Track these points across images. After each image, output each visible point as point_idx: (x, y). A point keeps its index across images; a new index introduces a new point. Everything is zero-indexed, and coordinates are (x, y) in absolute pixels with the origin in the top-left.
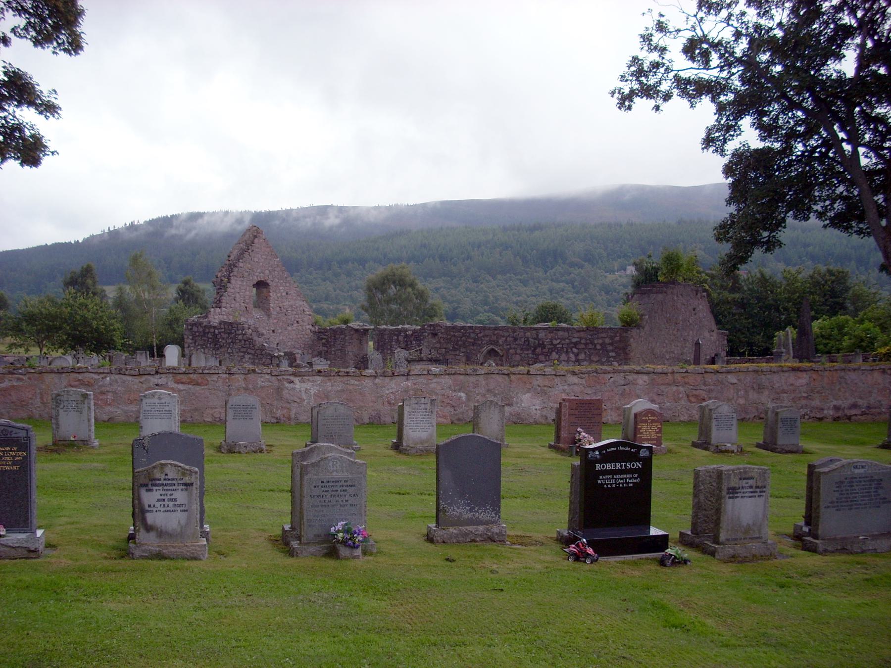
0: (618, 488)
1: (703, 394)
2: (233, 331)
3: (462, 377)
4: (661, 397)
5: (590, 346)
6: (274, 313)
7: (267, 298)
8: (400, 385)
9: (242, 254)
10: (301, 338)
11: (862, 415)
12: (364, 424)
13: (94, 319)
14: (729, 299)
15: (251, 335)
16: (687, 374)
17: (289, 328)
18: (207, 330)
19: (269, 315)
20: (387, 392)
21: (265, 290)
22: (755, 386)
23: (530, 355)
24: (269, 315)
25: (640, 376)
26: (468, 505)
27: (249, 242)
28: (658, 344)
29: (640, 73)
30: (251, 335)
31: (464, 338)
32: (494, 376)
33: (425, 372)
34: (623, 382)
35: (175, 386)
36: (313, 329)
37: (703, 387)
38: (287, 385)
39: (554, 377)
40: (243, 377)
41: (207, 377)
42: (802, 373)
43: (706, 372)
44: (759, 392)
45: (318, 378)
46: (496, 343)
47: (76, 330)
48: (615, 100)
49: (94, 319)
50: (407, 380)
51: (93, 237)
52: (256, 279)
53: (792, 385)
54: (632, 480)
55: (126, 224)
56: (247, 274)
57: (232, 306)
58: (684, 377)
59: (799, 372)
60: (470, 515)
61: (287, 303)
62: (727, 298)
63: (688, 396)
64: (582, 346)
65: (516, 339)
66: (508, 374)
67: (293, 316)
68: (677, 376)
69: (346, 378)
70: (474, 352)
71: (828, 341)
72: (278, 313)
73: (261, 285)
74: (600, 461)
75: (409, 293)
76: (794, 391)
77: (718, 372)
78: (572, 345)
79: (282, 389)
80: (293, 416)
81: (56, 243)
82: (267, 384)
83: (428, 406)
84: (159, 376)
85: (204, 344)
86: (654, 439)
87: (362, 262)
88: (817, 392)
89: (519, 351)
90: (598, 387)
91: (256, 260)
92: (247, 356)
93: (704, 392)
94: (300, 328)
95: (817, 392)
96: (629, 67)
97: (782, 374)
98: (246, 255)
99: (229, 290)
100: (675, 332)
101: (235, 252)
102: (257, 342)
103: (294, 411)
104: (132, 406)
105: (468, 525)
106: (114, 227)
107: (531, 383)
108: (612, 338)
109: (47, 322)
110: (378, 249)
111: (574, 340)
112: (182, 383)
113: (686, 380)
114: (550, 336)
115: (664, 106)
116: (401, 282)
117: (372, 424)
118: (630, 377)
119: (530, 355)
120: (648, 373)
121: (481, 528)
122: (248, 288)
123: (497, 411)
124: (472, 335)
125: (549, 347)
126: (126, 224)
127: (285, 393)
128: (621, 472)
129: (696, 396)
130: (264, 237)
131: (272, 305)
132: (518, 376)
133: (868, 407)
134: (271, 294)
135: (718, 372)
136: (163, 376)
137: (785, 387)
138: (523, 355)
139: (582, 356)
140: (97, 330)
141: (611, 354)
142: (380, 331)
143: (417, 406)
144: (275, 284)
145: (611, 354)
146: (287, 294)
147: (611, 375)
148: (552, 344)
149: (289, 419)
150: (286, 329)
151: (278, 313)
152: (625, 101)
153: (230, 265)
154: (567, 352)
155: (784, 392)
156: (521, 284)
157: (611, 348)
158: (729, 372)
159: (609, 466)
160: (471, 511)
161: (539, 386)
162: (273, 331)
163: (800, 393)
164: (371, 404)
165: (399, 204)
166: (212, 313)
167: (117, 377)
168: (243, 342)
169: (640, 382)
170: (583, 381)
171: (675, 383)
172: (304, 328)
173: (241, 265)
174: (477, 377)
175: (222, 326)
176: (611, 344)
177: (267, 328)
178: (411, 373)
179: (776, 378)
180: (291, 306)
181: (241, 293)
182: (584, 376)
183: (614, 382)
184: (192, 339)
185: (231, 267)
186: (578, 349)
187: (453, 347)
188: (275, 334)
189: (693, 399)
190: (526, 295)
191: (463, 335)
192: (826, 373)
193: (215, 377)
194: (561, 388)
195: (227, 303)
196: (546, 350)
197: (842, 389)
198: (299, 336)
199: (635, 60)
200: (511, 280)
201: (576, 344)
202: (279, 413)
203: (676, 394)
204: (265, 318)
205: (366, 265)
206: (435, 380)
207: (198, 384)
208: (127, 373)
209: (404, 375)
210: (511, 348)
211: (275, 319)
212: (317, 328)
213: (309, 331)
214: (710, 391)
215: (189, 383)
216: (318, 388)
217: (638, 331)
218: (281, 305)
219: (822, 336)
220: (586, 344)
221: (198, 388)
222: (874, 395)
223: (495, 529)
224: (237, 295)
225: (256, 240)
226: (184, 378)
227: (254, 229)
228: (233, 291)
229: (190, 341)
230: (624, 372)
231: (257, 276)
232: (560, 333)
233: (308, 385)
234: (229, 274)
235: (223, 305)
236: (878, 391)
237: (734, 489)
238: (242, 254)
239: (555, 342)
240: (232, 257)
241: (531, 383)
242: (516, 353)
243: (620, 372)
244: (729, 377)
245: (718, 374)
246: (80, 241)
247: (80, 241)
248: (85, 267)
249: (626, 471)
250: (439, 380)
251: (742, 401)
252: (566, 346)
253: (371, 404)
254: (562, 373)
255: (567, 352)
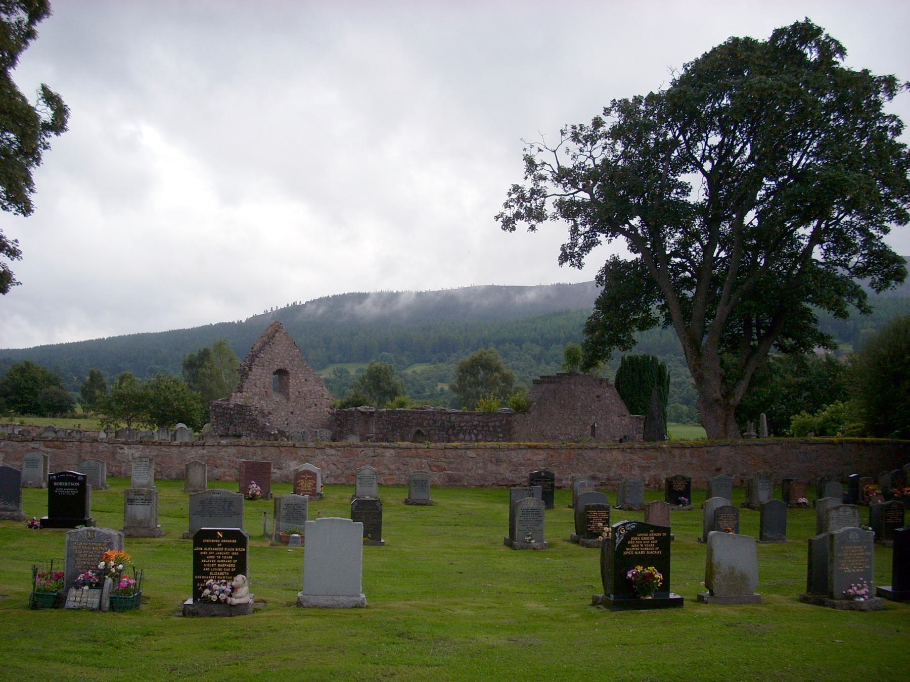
0: (66, 495)
1: (444, 465)
2: (243, 412)
3: (243, 448)
4: (406, 467)
5: (486, 428)
6: (292, 397)
7: (287, 385)
8: (198, 452)
9: (264, 346)
10: (319, 419)
11: (601, 485)
12: (172, 479)
13: (176, 400)
14: (792, 382)
15: (257, 416)
16: (428, 450)
17: (307, 410)
18: (226, 412)
19: (288, 399)
20: (189, 457)
21: (285, 377)
22: (493, 459)
23: (445, 436)
24: (288, 399)
25: (388, 450)
26: (3, 501)
27: (271, 336)
28: (549, 427)
29: (522, 198)
30: (257, 416)
31: (399, 421)
32: (267, 447)
33: (216, 444)
34: (372, 455)
35: (44, 449)
36: (331, 411)
37: (444, 460)
38: (119, 450)
39: (315, 449)
40: (89, 444)
41: (66, 444)
42: (539, 450)
43: (445, 448)
44: (497, 465)
45: (139, 446)
46: (421, 425)
47: (159, 409)
48: (500, 223)
49: (176, 400)
50: (203, 449)
51: (255, 318)
52: (276, 368)
53: (529, 460)
54: (74, 492)
55: (288, 305)
56: (267, 363)
57: (253, 390)
58: (426, 452)
59: (536, 450)
60: (4, 506)
61: (306, 388)
62: (791, 381)
63: (430, 466)
64: (480, 428)
65: (435, 422)
66: (278, 447)
67: (311, 400)
68: (420, 450)
69: (159, 447)
70: (406, 432)
71: (837, 425)
72: (297, 397)
73: (281, 373)
74: (57, 481)
75: (496, 377)
76: (532, 465)
77: (457, 448)
78: (473, 427)
79: (116, 453)
80: (123, 472)
81: (220, 324)
82: (105, 449)
83: (148, 463)
84: (34, 442)
85: (223, 423)
86: (310, 491)
87: (519, 342)
88: (555, 466)
89: (437, 432)
90: (352, 457)
91: (276, 351)
92: (252, 434)
93: (445, 464)
94: (318, 410)
95: (555, 466)
96: (510, 194)
97: (519, 451)
98: (267, 347)
99: (250, 377)
100: (571, 417)
101: (258, 345)
102: (260, 422)
103: (123, 469)
104: (17, 462)
105: (3, 511)
106: (277, 308)
107: (296, 454)
108: (501, 421)
109: (133, 402)
110: (535, 330)
111: (475, 423)
112: (49, 447)
113: (428, 454)
114: (458, 419)
115: (539, 226)
116: (486, 365)
117: (178, 479)
118: (379, 451)
119: (445, 436)
120: (394, 448)
121: (9, 513)
122: (268, 376)
123: (200, 468)
124: (405, 418)
125: (458, 428)
126: (288, 305)
127: (118, 456)
128: (67, 487)
129: (438, 466)
130: (284, 332)
131: (291, 390)
132: (287, 448)
133: (608, 479)
134: (290, 381)
135: (457, 448)
136: (37, 442)
137: (523, 462)
138: (440, 435)
139: (480, 437)
140: (178, 410)
141: (499, 435)
142: (379, 414)
143: (140, 463)
144: (294, 372)
145: (499, 435)
146: (306, 380)
147: (363, 449)
148: (460, 426)
149: (120, 473)
150: (304, 411)
151: (297, 397)
152: (508, 224)
153: (253, 355)
154: (470, 434)
155: (521, 465)
156: (682, 365)
157: (499, 430)
158: (467, 449)
159: (61, 484)
160: (4, 504)
161: (303, 456)
162: (292, 413)
163: (538, 466)
164: (177, 465)
165: (561, 283)
166: (233, 397)
167: (8, 442)
168: (250, 422)
169: (388, 454)
170: (340, 453)
171: (418, 456)
172: (322, 410)
173: (262, 355)
174: (256, 449)
175: (236, 408)
176: (500, 427)
177: (286, 410)
178: (206, 444)
179: (513, 454)
180: (310, 391)
181: (262, 380)
182: (340, 449)
183: (365, 454)
184: (215, 419)
185: (253, 357)
186: (477, 430)
187: (392, 428)
188: (293, 415)
189: (434, 469)
190: (686, 376)
191: (399, 418)
192: (563, 451)
193: (71, 444)
194: (322, 457)
195: (248, 388)
196: (455, 431)
197: (580, 464)
198: (316, 418)
199: (516, 188)
200: (670, 360)
201: (476, 426)
202: (114, 470)
203: (419, 464)
204: (284, 401)
205: (523, 345)
206: (224, 450)
207: (60, 448)
208: (14, 440)
209: (200, 446)
210: (431, 430)
211: (294, 402)
212: (335, 410)
213: (327, 413)
214: (450, 463)
215: (54, 448)
216: (140, 453)
217: (522, 416)
218: (300, 390)
219: (833, 420)
220: (483, 427)
221: (60, 451)
222: (613, 470)
223: (16, 514)
224: (258, 382)
225: (277, 335)
226: (51, 444)
227: (277, 324)
228: (253, 378)
229: (214, 420)
230: (373, 446)
231: (277, 365)
232: (466, 417)
233: (133, 451)
234: (251, 364)
235: (245, 389)
236: (618, 466)
237: (131, 500)
238: (264, 346)
239: (462, 425)
240: (255, 349)
241: (296, 454)
242: (435, 434)
243: (370, 447)
244: (468, 452)
245: (457, 450)
246: (243, 321)
247: (243, 321)
248: (202, 350)
249: (71, 487)
250: (226, 450)
251: (481, 472)
252: (469, 428)
253: (177, 465)
254: (321, 446)
255: (470, 434)
